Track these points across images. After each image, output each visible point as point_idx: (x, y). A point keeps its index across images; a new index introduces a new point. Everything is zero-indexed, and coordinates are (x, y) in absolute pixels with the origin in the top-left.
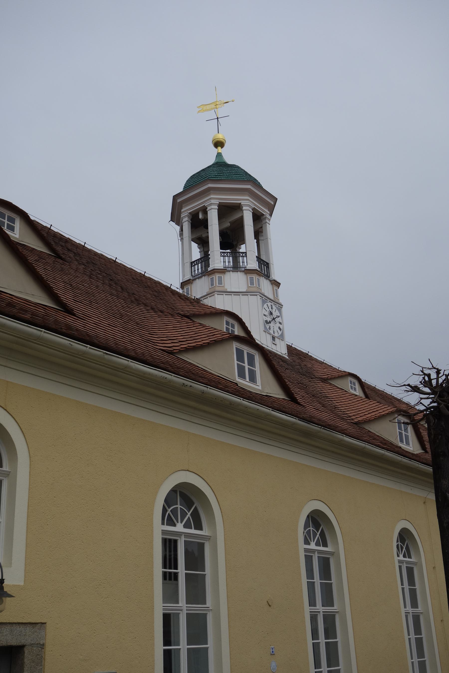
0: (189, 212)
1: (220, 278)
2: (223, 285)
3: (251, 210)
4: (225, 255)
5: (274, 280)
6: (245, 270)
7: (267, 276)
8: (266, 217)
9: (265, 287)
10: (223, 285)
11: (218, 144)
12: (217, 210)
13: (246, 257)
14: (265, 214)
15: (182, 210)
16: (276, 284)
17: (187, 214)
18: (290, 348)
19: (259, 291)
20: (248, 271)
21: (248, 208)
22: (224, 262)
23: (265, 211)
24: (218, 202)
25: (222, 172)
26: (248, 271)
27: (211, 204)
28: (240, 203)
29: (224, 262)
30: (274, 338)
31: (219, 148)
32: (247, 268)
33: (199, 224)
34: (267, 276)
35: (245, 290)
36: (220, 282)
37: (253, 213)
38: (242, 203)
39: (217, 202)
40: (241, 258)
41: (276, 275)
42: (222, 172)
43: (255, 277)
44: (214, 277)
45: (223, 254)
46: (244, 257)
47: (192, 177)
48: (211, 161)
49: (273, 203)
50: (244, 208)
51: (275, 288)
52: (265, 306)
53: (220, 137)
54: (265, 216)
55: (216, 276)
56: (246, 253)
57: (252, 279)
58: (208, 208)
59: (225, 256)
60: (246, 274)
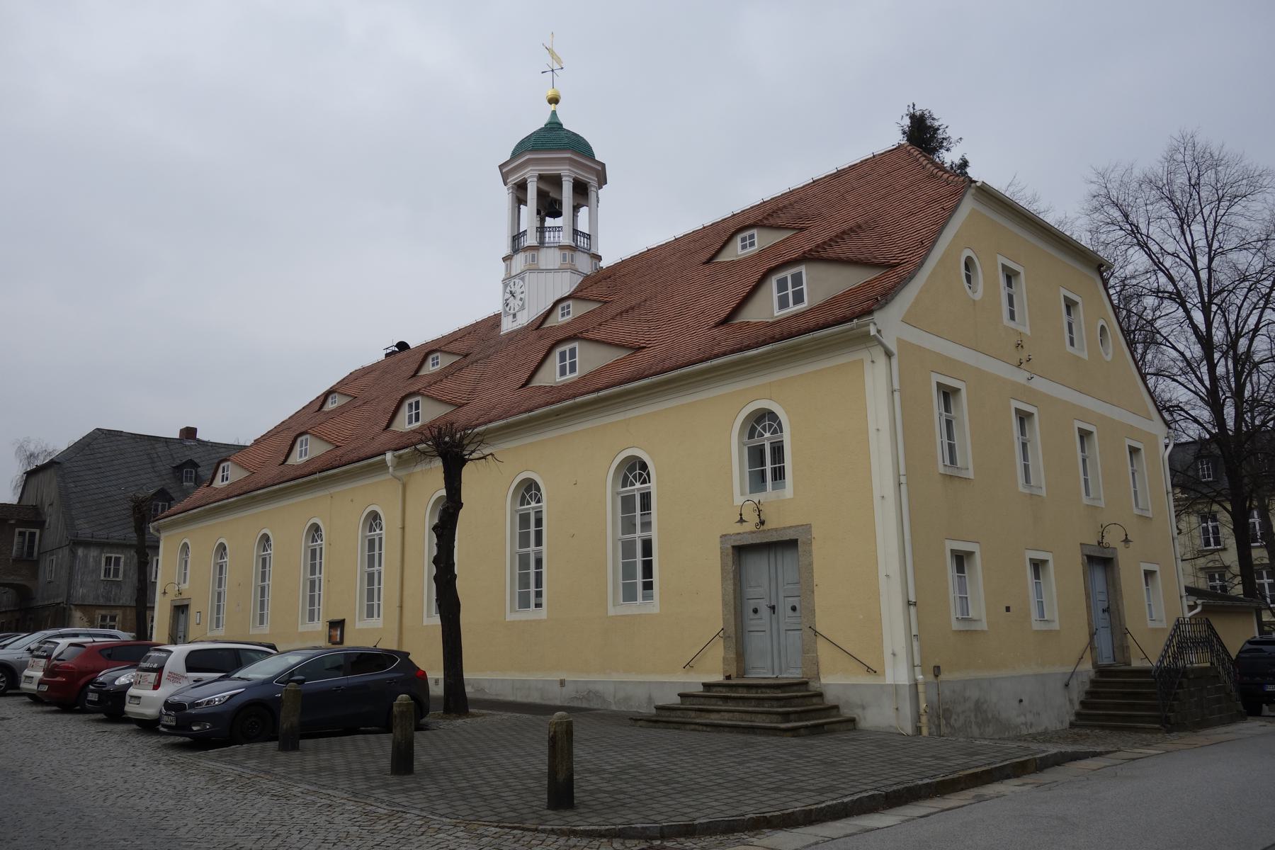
20: (562, 248)
23: (592, 180)
25: (552, 138)
33: (520, 200)
39: (536, 173)
42: (552, 138)
43: (567, 252)
53: (550, 93)
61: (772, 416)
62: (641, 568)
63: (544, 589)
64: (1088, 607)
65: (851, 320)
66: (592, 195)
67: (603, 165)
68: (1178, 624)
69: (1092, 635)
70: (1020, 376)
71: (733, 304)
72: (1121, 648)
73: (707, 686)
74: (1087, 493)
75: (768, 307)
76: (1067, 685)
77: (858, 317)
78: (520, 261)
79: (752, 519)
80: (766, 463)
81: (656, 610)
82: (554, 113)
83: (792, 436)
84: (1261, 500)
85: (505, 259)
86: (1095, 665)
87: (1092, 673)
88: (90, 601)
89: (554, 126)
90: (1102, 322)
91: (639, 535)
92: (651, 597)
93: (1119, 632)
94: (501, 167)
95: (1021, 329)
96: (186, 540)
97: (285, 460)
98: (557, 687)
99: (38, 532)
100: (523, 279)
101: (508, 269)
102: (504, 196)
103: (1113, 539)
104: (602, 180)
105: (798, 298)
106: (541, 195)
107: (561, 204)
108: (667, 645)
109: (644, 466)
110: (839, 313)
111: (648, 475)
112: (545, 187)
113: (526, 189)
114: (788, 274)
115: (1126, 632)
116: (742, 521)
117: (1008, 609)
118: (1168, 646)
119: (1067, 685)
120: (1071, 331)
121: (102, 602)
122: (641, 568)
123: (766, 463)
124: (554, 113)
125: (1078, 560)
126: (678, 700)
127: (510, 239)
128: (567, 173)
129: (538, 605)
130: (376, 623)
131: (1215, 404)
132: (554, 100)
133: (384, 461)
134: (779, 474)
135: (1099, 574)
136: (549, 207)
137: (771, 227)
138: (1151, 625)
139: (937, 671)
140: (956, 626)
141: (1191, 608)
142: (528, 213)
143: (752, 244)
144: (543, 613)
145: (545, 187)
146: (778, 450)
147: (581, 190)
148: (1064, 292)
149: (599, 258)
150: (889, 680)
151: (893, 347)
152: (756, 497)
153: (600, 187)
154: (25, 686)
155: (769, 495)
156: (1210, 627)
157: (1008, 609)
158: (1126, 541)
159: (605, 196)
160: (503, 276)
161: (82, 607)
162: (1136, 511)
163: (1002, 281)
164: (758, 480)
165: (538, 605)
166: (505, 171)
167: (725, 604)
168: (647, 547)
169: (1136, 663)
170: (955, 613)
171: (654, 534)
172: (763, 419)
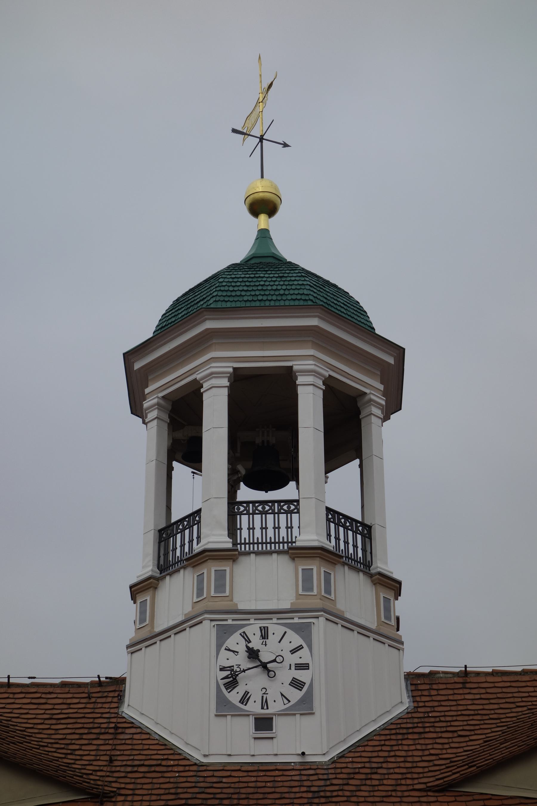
0: (161, 395)
1: (220, 576)
2: (227, 593)
3: (320, 383)
4: (267, 508)
5: (380, 574)
6: (289, 548)
7: (364, 566)
8: (371, 400)
9: (354, 594)
10: (227, 593)
11: (263, 206)
12: (225, 391)
13: (298, 512)
14: (367, 391)
15: (147, 391)
16: (394, 586)
17: (155, 401)
18: (106, 678)
19: (328, 606)
20: (297, 553)
21: (310, 379)
22: (289, 528)
23: (372, 387)
24: (231, 370)
25: (265, 282)
26: (297, 553)
27: (211, 375)
28: (291, 367)
29: (289, 528)
30: (264, 724)
31: (263, 217)
32: (298, 544)
33: (185, 448)
34: (364, 566)
35: (286, 605)
36: (220, 586)
37: (325, 392)
38: (295, 368)
39: (228, 368)
40: (245, 518)
41: (391, 559)
42: (265, 282)
43: (317, 568)
44: (205, 571)
45: (285, 507)
46: (292, 512)
47: (178, 302)
48: (239, 250)
49: (391, 361)
50: (300, 380)
51: (382, 596)
52: (234, 641)
53: (260, 188)
54: (367, 398)
55: (210, 570)
56: (298, 501)
57: (307, 576)
58: (206, 386)
59: (266, 513)
60: (293, 559)
67: (399, 352)
78: (177, 595)
82: (264, 235)
85: (137, 590)
94: (131, 587)
99: (300, 592)
100: (304, 631)
101: (144, 616)
102: (142, 440)
124: (264, 235)
127: (151, 537)
128: (310, 365)
132: (263, 206)
136: (262, 455)
142: (200, 489)
153: (386, 418)
159: (390, 437)
160: (129, 633)
166: (139, 368)
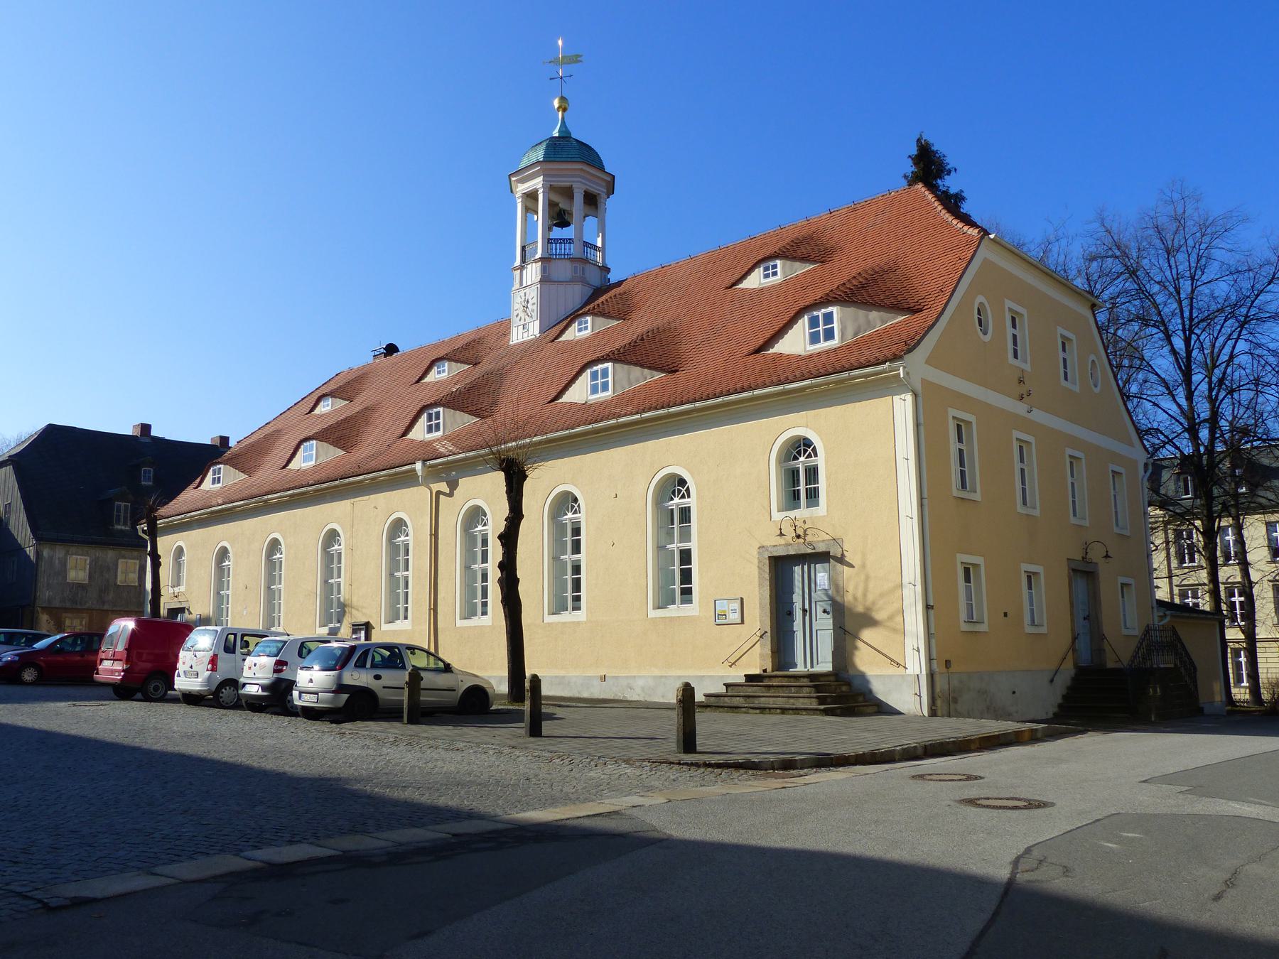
20: (572, 260)
43: (579, 265)
61: (808, 443)
62: (678, 580)
63: (583, 593)
64: (1072, 614)
65: (884, 362)
66: (601, 206)
68: (1148, 630)
69: (1074, 639)
70: (1020, 408)
71: (767, 335)
72: (1098, 651)
73: (750, 678)
74: (1075, 515)
75: (796, 343)
76: (1052, 681)
77: (891, 360)
79: (790, 534)
80: (799, 481)
81: (696, 613)
83: (827, 461)
84: (1236, 518)
86: (1076, 666)
87: (1072, 672)
88: (57, 604)
89: (565, 137)
90: (1093, 357)
91: (676, 546)
92: (579, 608)
93: (1097, 636)
95: (1023, 366)
96: (181, 543)
97: (287, 465)
98: (597, 682)
103: (1096, 554)
104: (611, 190)
105: (829, 335)
106: (551, 205)
107: (571, 214)
108: (716, 645)
109: (682, 482)
110: (869, 354)
111: (688, 490)
112: (556, 198)
113: (537, 200)
114: (820, 313)
115: (1103, 637)
116: (781, 534)
117: (1006, 614)
118: (1139, 648)
119: (1052, 681)
120: (1065, 367)
121: (68, 605)
122: (678, 580)
123: (799, 481)
125: (1064, 571)
126: (724, 690)
129: (484, 613)
130: (400, 625)
131: (1193, 431)
133: (414, 470)
134: (813, 495)
135: (1081, 584)
137: (794, 259)
138: (1125, 632)
139: (948, 663)
140: (965, 627)
141: (1162, 618)
143: (775, 274)
144: (581, 616)
145: (556, 198)
146: (812, 473)
147: (592, 201)
148: (1060, 330)
149: (608, 270)
150: (909, 672)
151: (919, 387)
152: (792, 514)
154: (101, 677)
155: (803, 513)
156: (1175, 633)
157: (1006, 614)
158: (1107, 556)
159: (611, 205)
161: (49, 610)
162: (1116, 530)
163: (1009, 323)
164: (793, 499)
165: (406, 618)
167: (762, 607)
168: (686, 556)
169: (1111, 664)
170: (963, 615)
171: (693, 545)
172: (801, 446)
